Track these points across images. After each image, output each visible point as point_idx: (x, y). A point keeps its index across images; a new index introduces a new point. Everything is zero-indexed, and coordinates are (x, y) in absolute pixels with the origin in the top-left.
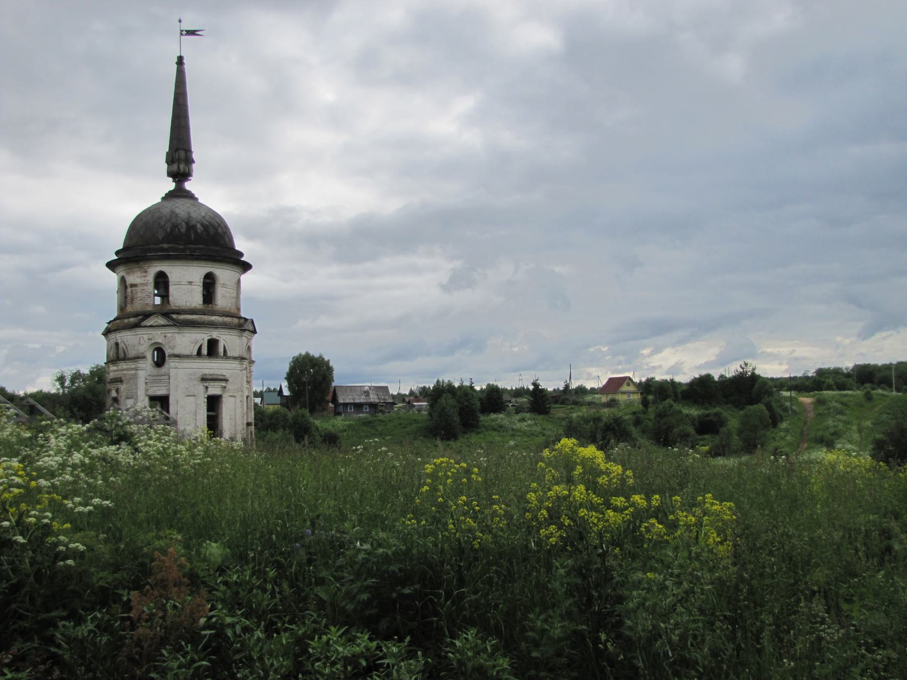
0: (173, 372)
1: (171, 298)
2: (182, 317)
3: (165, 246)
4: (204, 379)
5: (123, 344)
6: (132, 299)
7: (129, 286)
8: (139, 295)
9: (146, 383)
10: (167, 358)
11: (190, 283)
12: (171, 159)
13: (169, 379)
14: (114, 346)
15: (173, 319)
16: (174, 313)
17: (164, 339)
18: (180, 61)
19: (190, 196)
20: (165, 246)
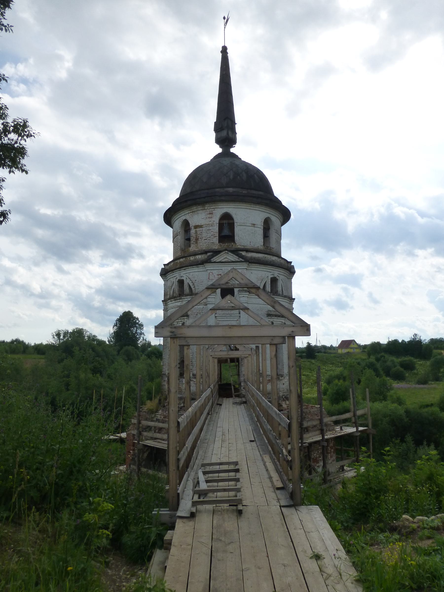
1: (236, 238)
2: (250, 255)
3: (231, 190)
5: (188, 281)
6: (197, 239)
7: (193, 228)
8: (204, 235)
9: (216, 317)
12: (218, 128)
16: (243, 250)
18: (224, 50)
19: (234, 156)
20: (231, 190)
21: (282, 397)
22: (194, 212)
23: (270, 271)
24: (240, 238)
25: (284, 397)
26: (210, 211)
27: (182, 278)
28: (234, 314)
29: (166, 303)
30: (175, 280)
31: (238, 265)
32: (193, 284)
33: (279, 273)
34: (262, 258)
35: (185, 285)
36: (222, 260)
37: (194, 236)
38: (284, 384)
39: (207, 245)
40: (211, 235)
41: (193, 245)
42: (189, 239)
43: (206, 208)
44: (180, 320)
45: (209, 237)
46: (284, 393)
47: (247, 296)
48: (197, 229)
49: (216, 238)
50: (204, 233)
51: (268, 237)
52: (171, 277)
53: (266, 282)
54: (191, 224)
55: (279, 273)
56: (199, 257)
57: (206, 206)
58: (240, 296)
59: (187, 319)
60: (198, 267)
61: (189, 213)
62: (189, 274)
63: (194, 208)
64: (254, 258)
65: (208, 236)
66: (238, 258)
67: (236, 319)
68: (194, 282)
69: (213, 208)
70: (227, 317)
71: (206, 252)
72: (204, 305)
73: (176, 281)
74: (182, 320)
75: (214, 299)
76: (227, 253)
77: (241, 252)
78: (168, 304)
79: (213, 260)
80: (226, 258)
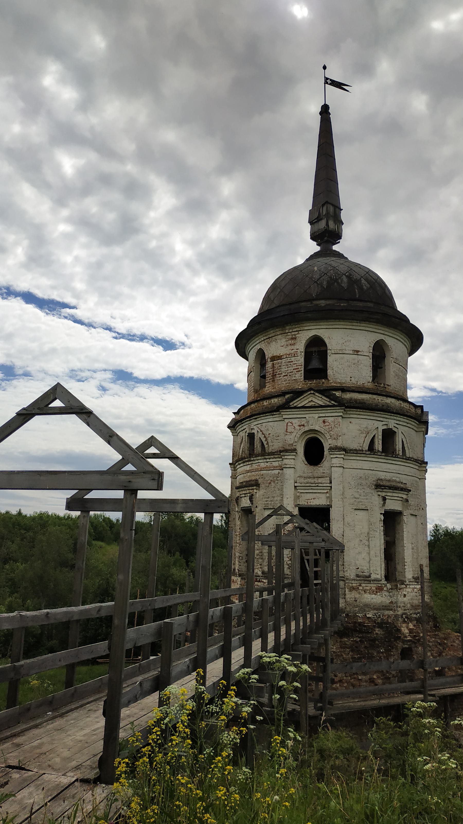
0: (336, 473)
1: (330, 372)
2: (348, 396)
3: (322, 303)
4: (379, 486)
5: (260, 435)
6: (274, 376)
7: (269, 360)
8: (284, 369)
9: (295, 487)
10: (326, 452)
11: (356, 352)
13: (331, 483)
14: (246, 439)
15: (335, 399)
16: (337, 389)
17: (322, 425)
18: (325, 110)
19: (339, 255)
20: (322, 303)
21: (402, 617)
22: (271, 337)
23: (382, 419)
24: (335, 372)
25: (404, 616)
26: (293, 335)
27: (253, 431)
28: (321, 483)
29: (235, 467)
30: (244, 434)
31: (328, 411)
32: (266, 440)
33: (398, 422)
34: (367, 400)
35: (255, 440)
36: (305, 404)
37: (270, 372)
38: (405, 596)
39: (288, 383)
40: (294, 369)
41: (268, 384)
42: (264, 377)
43: (287, 331)
44: (248, 492)
45: (291, 372)
46: (405, 610)
47: (343, 456)
48: (274, 362)
49: (300, 373)
50: (284, 367)
51: (382, 368)
52: (240, 430)
53: (374, 436)
54: (267, 354)
55: (398, 422)
56: (275, 401)
57: (287, 328)
58: (332, 456)
59: (256, 489)
60: (273, 415)
61: (264, 340)
62: (261, 426)
63: (271, 333)
64: (356, 400)
65: (290, 371)
66: (328, 400)
67: (326, 491)
68: (267, 436)
69: (297, 331)
70: (313, 488)
71: (283, 394)
72: (280, 469)
73: (245, 436)
74: (251, 491)
75: (292, 461)
76: (313, 394)
77: (334, 392)
78: (237, 467)
79: (293, 404)
80: (312, 401)
